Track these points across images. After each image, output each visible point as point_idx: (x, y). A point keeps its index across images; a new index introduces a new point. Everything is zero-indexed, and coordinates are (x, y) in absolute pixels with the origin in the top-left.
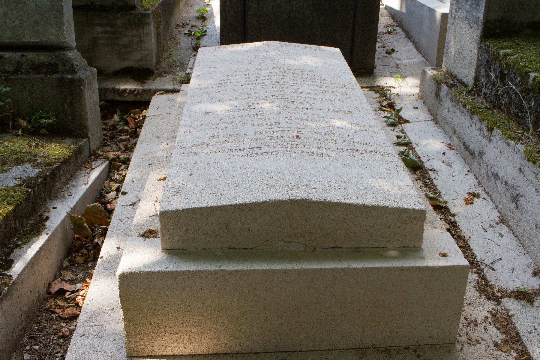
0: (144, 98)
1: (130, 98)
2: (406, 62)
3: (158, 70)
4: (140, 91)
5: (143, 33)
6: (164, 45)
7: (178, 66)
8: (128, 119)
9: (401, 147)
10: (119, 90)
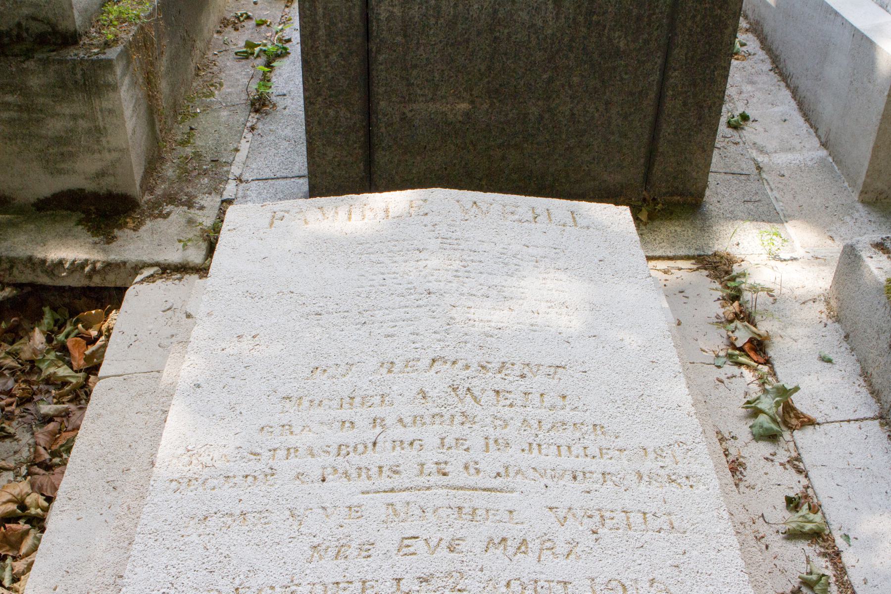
0: (112, 280)
1: (77, 281)
2: (782, 159)
3: (151, 190)
4: (99, 265)
5: (101, 110)
6: (166, 118)
7: (205, 172)
8: (70, 343)
10: (43, 261)
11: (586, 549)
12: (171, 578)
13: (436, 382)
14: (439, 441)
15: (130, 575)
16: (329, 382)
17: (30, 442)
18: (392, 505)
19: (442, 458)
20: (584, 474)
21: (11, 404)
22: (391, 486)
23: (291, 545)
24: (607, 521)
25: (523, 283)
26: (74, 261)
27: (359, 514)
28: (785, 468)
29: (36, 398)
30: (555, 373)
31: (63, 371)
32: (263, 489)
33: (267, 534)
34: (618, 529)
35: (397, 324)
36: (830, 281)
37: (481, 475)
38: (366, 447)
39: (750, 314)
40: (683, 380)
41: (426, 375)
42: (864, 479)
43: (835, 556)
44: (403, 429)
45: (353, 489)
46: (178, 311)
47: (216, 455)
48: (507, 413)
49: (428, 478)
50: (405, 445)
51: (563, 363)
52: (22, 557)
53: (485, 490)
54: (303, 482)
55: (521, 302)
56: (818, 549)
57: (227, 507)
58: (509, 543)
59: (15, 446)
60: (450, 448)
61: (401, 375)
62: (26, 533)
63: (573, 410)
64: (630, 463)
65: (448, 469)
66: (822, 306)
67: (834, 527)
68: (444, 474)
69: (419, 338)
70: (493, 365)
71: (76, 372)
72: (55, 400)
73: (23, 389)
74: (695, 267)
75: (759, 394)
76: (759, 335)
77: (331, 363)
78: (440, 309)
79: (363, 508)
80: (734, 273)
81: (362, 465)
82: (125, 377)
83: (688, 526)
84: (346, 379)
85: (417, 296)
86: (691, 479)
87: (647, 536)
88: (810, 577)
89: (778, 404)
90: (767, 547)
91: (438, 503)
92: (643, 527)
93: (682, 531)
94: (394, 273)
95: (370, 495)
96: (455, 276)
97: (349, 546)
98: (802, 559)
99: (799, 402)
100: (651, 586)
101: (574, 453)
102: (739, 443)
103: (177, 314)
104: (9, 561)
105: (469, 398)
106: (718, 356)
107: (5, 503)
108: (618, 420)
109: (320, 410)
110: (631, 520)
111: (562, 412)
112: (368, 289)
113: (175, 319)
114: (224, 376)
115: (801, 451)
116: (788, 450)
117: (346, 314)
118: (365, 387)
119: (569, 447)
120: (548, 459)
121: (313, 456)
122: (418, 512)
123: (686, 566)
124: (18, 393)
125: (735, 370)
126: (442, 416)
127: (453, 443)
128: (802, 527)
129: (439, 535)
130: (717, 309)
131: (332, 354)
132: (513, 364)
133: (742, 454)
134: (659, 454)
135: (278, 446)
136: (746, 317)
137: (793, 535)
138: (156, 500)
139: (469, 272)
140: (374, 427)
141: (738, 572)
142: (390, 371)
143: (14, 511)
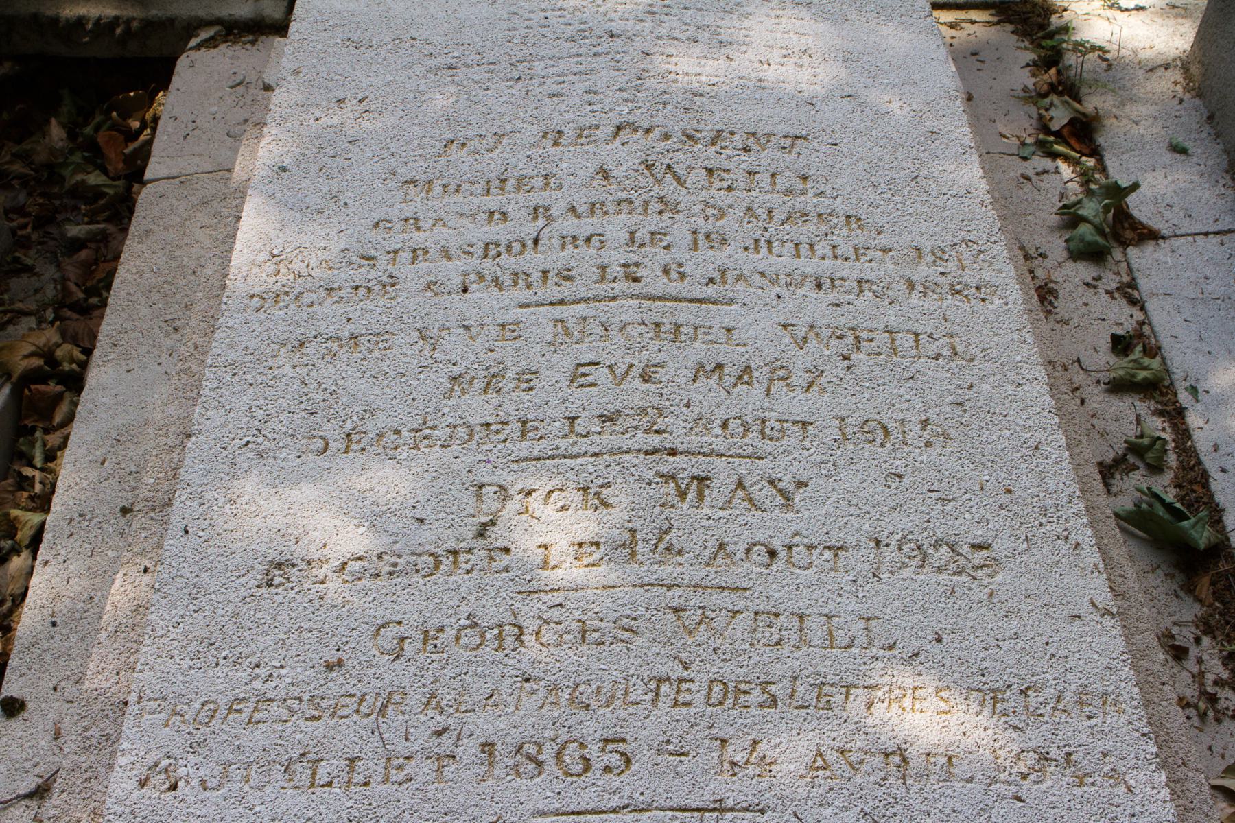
4: (135, 24)
8: (101, 138)
9: (1128, 400)
11: (834, 379)
13: (622, 158)
14: (627, 236)
15: (201, 421)
16: (469, 160)
17: (55, 276)
19: (632, 258)
20: (832, 281)
21: (24, 227)
22: (560, 296)
23: (422, 376)
25: (746, 23)
26: (100, 19)
27: (516, 334)
28: (1113, 298)
29: (60, 217)
30: (793, 146)
31: (94, 179)
32: (381, 303)
33: (388, 362)
34: (879, 354)
35: (565, 79)
36: (1192, 40)
37: (686, 281)
38: (524, 246)
39: (1073, 85)
40: (975, 157)
41: (609, 147)
42: (1223, 313)
43: (1176, 415)
44: (576, 221)
45: (507, 302)
46: (253, 86)
47: (313, 261)
48: (724, 198)
49: (612, 285)
50: (580, 242)
51: (804, 133)
52: (55, 429)
53: (692, 301)
54: (436, 294)
55: (744, 48)
56: (1153, 405)
57: (331, 329)
58: (726, 371)
60: (642, 245)
61: (571, 148)
62: (59, 398)
63: (816, 195)
64: (898, 267)
65: (640, 272)
66: (1178, 76)
67: (1178, 375)
68: (636, 280)
69: (597, 98)
70: (703, 134)
71: (113, 179)
72: (86, 219)
73: (40, 205)
74: (995, 19)
75: (1080, 196)
76: (1084, 115)
77: (471, 134)
78: (628, 58)
79: (521, 326)
80: (1052, 28)
81: (519, 269)
82: (182, 179)
84: (494, 155)
85: (594, 41)
86: (984, 289)
87: (919, 365)
88: (1140, 440)
89: (1106, 209)
90: (1083, 402)
91: (625, 318)
92: (915, 352)
93: (968, 358)
94: (561, 9)
95: (531, 309)
96: (649, 13)
97: (503, 377)
98: (1128, 418)
99: (1138, 206)
100: (924, 429)
101: (819, 252)
102: (1050, 263)
103: (251, 91)
104: (38, 434)
105: (669, 178)
106: (1023, 144)
107: (26, 357)
108: (881, 209)
109: (458, 198)
110: (897, 343)
111: (802, 198)
112: (523, 31)
113: (248, 99)
114: (320, 155)
115: (1136, 274)
117: (492, 67)
118: (521, 165)
119: (812, 246)
120: (784, 261)
121: (449, 258)
122: (598, 330)
124: (34, 210)
125: (1048, 163)
126: (631, 203)
127: (648, 238)
128: (1133, 376)
129: (628, 360)
130: (1024, 79)
131: (474, 122)
132: (732, 133)
134: (938, 256)
135: (399, 246)
136: (1068, 89)
137: (1118, 387)
138: (231, 322)
139: (669, 6)
140: (536, 218)
141: (1045, 413)
142: (556, 144)
143: (39, 368)
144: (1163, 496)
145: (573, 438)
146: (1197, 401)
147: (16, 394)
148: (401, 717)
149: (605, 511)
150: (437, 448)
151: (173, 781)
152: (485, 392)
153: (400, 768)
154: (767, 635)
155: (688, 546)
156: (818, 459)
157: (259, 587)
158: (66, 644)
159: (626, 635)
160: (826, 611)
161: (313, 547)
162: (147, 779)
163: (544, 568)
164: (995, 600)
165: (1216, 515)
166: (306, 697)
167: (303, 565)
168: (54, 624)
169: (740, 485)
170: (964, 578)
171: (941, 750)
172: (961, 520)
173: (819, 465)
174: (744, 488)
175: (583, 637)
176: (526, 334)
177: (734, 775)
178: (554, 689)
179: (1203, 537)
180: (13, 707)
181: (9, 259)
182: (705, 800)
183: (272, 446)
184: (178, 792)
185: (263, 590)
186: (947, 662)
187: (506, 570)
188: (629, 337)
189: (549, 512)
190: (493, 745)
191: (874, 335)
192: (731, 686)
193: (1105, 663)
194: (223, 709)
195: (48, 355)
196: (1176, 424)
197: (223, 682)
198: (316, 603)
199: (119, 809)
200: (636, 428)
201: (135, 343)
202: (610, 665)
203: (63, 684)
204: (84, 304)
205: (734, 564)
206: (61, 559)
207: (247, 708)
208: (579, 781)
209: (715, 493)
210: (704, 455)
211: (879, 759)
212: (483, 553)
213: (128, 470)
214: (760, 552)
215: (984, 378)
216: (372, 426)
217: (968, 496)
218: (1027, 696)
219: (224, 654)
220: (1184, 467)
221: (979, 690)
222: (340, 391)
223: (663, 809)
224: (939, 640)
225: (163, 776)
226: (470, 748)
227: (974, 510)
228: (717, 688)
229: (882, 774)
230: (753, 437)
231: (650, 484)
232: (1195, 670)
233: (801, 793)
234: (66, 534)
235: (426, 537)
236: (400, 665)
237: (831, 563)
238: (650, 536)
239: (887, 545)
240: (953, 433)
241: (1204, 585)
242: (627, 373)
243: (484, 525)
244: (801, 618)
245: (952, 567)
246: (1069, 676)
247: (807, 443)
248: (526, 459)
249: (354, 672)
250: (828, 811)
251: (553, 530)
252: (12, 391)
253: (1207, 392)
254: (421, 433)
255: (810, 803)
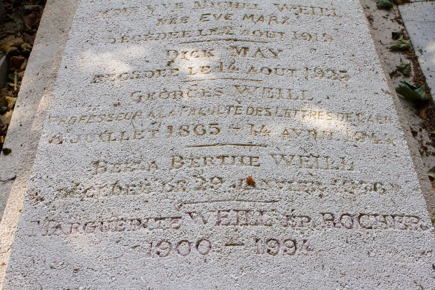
12: (91, 35)
15: (71, 35)
17: (21, 22)
18: (197, 2)
24: (303, 11)
28: (393, 22)
29: (22, 4)
34: (308, 14)
43: (415, 59)
56: (406, 56)
58: (255, 17)
59: (14, 24)
67: (415, 46)
79: (183, 4)
83: (343, 14)
87: (322, 17)
92: (321, 14)
98: (398, 59)
100: (324, 36)
104: (15, 72)
107: (11, 46)
115: (401, 14)
116: (395, 14)
123: (341, 29)
129: (220, 13)
133: (372, 15)
137: (394, 49)
138: (82, 6)
141: (367, 33)
143: (15, 50)
144: (410, 84)
145: (201, 36)
146: (422, 54)
147: (8, 59)
148: (140, 119)
149: (212, 57)
150: (154, 40)
151: (61, 141)
152: (170, 24)
153: (139, 134)
154: (268, 94)
155: (240, 67)
156: (286, 44)
157: (91, 83)
158: (25, 131)
159: (219, 93)
160: (289, 88)
161: (110, 70)
162: (52, 140)
163: (190, 74)
164: (348, 87)
165: (428, 90)
166: (107, 114)
167: (107, 76)
168: (21, 125)
169: (259, 50)
170: (337, 80)
171: (328, 131)
172: (336, 63)
173: (287, 45)
174: (260, 51)
175: (204, 94)
176: (184, 6)
177: (256, 135)
178: (194, 110)
179: (423, 95)
180: (7, 152)
181: (5, 16)
182: (246, 142)
183: (96, 41)
184: (63, 144)
185: (93, 84)
186: (331, 105)
187: (177, 75)
188: (221, 6)
189: (192, 58)
190: (172, 127)
191: (307, 8)
192: (255, 109)
193: (386, 107)
194: (78, 119)
195: (19, 46)
196: (414, 62)
197: (78, 111)
198: (111, 87)
199: (42, 150)
200: (223, 33)
201: (49, 37)
202: (214, 102)
203: (24, 144)
204: (30, 31)
205: (257, 73)
206: (23, 105)
207: (87, 119)
208: (202, 137)
209: (250, 52)
210: (246, 41)
211: (307, 133)
212: (169, 71)
213: (47, 77)
214: (266, 71)
215: (345, 22)
216: (131, 34)
217: (339, 56)
218: (359, 116)
219: (79, 103)
220: (417, 75)
221: (342, 114)
222: (120, 25)
223: (231, 144)
224: (328, 98)
225: (57, 139)
226: (164, 128)
227: (341, 61)
228: (250, 109)
229: (308, 137)
230: (264, 37)
231: (227, 49)
232: (420, 140)
233: (279, 141)
234: (25, 97)
235: (149, 66)
236: (139, 104)
237: (291, 74)
238: (227, 64)
239: (310, 70)
240: (334, 38)
241: (423, 113)
242: (220, 17)
243: (170, 62)
244: (280, 90)
245: (333, 77)
246: (373, 111)
247: (283, 39)
248: (185, 43)
249: (124, 107)
250: (289, 147)
251: (192, 63)
252: (6, 58)
253: (426, 51)
254: (148, 36)
255: (282, 144)
